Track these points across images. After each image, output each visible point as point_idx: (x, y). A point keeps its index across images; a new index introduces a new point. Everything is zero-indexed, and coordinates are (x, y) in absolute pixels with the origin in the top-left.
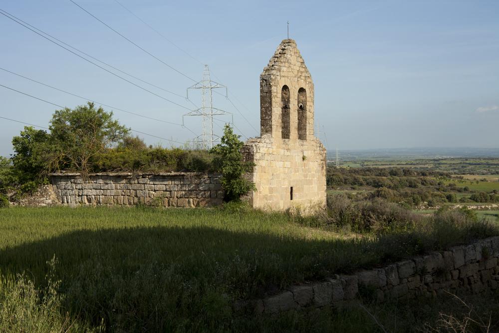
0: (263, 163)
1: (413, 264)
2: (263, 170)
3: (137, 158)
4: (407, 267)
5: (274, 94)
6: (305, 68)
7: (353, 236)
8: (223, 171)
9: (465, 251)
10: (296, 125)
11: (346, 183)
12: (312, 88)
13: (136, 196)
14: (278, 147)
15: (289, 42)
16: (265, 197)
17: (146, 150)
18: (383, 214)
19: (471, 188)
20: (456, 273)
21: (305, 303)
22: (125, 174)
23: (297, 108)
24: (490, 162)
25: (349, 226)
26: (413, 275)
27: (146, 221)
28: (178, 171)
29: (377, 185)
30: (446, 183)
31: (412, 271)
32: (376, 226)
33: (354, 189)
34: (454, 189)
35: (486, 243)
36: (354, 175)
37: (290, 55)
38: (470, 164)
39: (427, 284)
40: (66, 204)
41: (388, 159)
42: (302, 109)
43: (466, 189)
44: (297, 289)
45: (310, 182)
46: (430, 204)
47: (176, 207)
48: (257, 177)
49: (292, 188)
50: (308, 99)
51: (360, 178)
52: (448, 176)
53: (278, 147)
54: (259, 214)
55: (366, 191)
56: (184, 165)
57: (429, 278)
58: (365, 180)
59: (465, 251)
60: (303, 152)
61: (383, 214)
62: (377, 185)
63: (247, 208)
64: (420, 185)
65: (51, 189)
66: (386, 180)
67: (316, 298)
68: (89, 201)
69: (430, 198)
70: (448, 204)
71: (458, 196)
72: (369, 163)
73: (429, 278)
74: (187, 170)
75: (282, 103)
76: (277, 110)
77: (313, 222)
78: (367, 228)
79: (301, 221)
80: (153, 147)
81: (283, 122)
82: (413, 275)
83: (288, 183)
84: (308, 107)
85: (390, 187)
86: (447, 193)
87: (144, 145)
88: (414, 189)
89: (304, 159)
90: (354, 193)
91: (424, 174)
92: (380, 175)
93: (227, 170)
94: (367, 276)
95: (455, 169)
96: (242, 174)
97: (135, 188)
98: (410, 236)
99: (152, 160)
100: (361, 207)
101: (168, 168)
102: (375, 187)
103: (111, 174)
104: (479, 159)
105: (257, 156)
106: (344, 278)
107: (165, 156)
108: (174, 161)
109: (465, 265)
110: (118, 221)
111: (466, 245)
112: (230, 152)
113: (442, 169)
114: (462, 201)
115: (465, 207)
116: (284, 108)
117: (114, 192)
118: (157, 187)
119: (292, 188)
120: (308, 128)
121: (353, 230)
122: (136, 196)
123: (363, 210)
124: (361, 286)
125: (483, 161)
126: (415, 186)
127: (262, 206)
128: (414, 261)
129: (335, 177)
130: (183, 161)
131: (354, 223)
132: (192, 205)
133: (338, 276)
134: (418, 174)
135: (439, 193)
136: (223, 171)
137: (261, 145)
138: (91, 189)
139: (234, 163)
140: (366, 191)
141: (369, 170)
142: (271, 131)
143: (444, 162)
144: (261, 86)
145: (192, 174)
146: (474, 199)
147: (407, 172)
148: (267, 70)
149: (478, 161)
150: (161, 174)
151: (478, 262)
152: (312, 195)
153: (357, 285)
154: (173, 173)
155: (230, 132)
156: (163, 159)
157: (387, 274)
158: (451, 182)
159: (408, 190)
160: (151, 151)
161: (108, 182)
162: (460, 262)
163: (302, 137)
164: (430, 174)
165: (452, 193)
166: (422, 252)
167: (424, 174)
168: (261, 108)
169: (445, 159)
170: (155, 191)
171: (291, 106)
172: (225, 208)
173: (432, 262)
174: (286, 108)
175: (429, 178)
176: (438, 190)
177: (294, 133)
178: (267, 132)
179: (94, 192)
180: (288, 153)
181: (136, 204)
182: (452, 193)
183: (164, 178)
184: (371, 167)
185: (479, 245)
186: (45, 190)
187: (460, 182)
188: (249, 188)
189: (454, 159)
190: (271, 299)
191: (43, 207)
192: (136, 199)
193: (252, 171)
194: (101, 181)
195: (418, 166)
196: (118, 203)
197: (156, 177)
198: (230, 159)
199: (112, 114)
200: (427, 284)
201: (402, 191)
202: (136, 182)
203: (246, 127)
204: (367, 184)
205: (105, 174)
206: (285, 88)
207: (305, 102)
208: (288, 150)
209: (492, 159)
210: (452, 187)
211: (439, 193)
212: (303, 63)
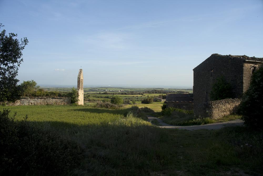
13: (47, 102)
22: (44, 97)
24: (64, 89)
38: (58, 90)
40: (23, 105)
61: (110, 105)
65: (19, 101)
68: (31, 104)
74: (62, 97)
103: (40, 97)
117: (40, 102)
122: (47, 102)
125: (62, 89)
138: (32, 101)
143: (51, 89)
149: (61, 89)
161: (38, 99)
168: (78, 83)
169: (51, 88)
179: (33, 102)
183: (55, 98)
186: (17, 101)
189: (53, 88)
191: (17, 106)
192: (47, 103)
193: (78, 97)
194: (36, 99)
196: (41, 104)
197: (53, 98)
199: (19, 81)
205: (38, 97)
209: (65, 88)
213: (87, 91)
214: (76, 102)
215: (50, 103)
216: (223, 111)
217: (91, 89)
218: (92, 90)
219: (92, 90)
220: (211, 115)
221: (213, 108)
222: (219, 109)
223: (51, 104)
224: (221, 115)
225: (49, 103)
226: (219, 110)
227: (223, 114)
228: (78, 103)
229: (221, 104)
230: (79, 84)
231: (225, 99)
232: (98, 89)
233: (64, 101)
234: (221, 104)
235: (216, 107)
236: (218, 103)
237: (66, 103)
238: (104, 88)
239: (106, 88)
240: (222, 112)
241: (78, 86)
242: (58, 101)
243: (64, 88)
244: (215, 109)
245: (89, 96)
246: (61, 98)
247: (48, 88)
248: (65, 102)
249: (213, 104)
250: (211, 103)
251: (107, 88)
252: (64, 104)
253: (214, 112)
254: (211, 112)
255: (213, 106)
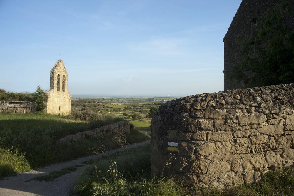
0: (51, 99)
1: (100, 129)
2: (51, 101)
3: (3, 96)
4: (99, 130)
5: (55, 77)
6: (65, 69)
7: (81, 121)
8: (37, 101)
9: (114, 125)
10: (62, 87)
11: (74, 105)
12: (67, 75)
13: (2, 109)
14: (56, 94)
15: (60, 61)
16: (51, 110)
17: (7, 93)
18: (90, 115)
19: (113, 107)
20: (112, 131)
21: (70, 141)
23: (62, 81)
24: (119, 99)
25: (79, 119)
26: (100, 132)
27: (7, 117)
28: (19, 101)
29: (84, 106)
30: (106, 105)
31: (100, 131)
32: (88, 118)
33: (76, 107)
34: (108, 107)
35: (120, 123)
36: (77, 103)
37: (60, 65)
38: (113, 100)
39: (104, 134)
41: (88, 98)
42: (64, 82)
43: (112, 107)
44: (68, 137)
45: (66, 105)
46: (101, 112)
47: (21, 112)
48: (48, 103)
49: (60, 107)
50: (66, 79)
51: (79, 103)
52: (107, 103)
53: (56, 94)
54: (49, 115)
55: (80, 108)
56: (21, 98)
57: (104, 133)
58: (80, 104)
59: (114, 125)
60: (64, 95)
61: (90, 115)
62: (84, 106)
63: (45, 113)
64: (98, 106)
66: (87, 104)
67: (73, 139)
69: (101, 110)
70: (106, 112)
71: (110, 110)
72: (82, 99)
73: (104, 133)
74: (23, 101)
75: (57, 80)
76: (56, 82)
77: (68, 117)
78: (85, 119)
79: (64, 117)
80: (9, 92)
81: (58, 86)
82: (100, 132)
83: (58, 105)
84: (66, 82)
85: (88, 107)
86: (106, 109)
87: (6, 92)
88: (96, 107)
89: (64, 98)
90: (77, 108)
91: (99, 103)
92: (85, 103)
93: (38, 100)
94: (88, 132)
95: (109, 101)
96: (43, 102)
97: (2, 106)
98: (99, 121)
99: (9, 97)
100: (83, 113)
101: (15, 100)
102: (84, 106)
104: (116, 98)
105: (49, 97)
106: (81, 133)
107: (14, 96)
108: (18, 97)
109: (114, 129)
110: (11, 117)
111: (115, 123)
112: (39, 95)
113: (105, 101)
114: (111, 111)
115: (112, 113)
116: (57, 81)
118: (11, 106)
119: (60, 107)
120: (65, 88)
121: (80, 120)
122: (2, 109)
123: (84, 114)
124: (86, 135)
125: (117, 99)
126: (96, 106)
127: (50, 113)
128: (100, 128)
129: (74, 103)
130: (22, 98)
131: (81, 118)
132: (25, 112)
133: (80, 133)
134: (97, 103)
135: (104, 109)
136: (37, 101)
137: (50, 93)
139: (41, 98)
140: (80, 108)
141: (82, 101)
142: (54, 88)
143: (105, 99)
144: (51, 74)
145: (25, 102)
146: (114, 111)
147: (94, 102)
148: (53, 69)
149: (116, 99)
150: (13, 102)
151: (118, 128)
152: (66, 109)
153: (85, 135)
154: (18, 102)
155: (40, 89)
156: (14, 96)
157: (93, 132)
158: (108, 105)
159: (94, 108)
160: (9, 94)
162: (113, 128)
163: (64, 91)
164: (101, 103)
165: (108, 109)
166: (102, 125)
167: (99, 103)
168: (51, 81)
170: (10, 107)
171: (60, 81)
172: (37, 113)
173: (105, 128)
174: (59, 81)
175: (101, 104)
176: (103, 107)
177: (61, 89)
178: (52, 89)
180: (59, 96)
181: (2, 112)
182: (108, 109)
183: (14, 103)
184: (82, 100)
185: (118, 123)
187: (110, 105)
188: (45, 107)
189: (108, 98)
190: (60, 139)
192: (2, 110)
193: (47, 101)
195: (97, 100)
197: (10, 103)
198: (40, 97)
200: (104, 134)
201: (92, 108)
202: (2, 104)
203: (45, 87)
204: (81, 106)
206: (59, 75)
207: (65, 80)
208: (59, 95)
209: (120, 98)
210: (108, 107)
211: (104, 109)
212: (65, 67)
213: (144, 102)
214: (42, 109)
215: (7, 111)
216: (264, 149)
217: (147, 99)
218: (149, 101)
219: (149, 101)
220: (190, 163)
221: (201, 129)
222: (239, 133)
223: (8, 112)
224: (249, 166)
225: (4, 110)
226: (235, 141)
227: (259, 161)
228: (47, 110)
229: (249, 112)
230: (52, 81)
231: (277, 87)
232: (155, 99)
233: (26, 107)
234: (249, 112)
235: (220, 122)
236: (232, 104)
237: (30, 111)
238: (163, 98)
239: (164, 98)
240: (258, 151)
241: (51, 84)
242: (19, 107)
243: (119, 98)
244: (216, 137)
245: (143, 107)
246: (21, 103)
247: (102, 98)
248: (28, 109)
249: (203, 110)
250: (192, 106)
251: (166, 98)
252: (27, 112)
253: (208, 149)
254: (190, 149)
255: (202, 121)
